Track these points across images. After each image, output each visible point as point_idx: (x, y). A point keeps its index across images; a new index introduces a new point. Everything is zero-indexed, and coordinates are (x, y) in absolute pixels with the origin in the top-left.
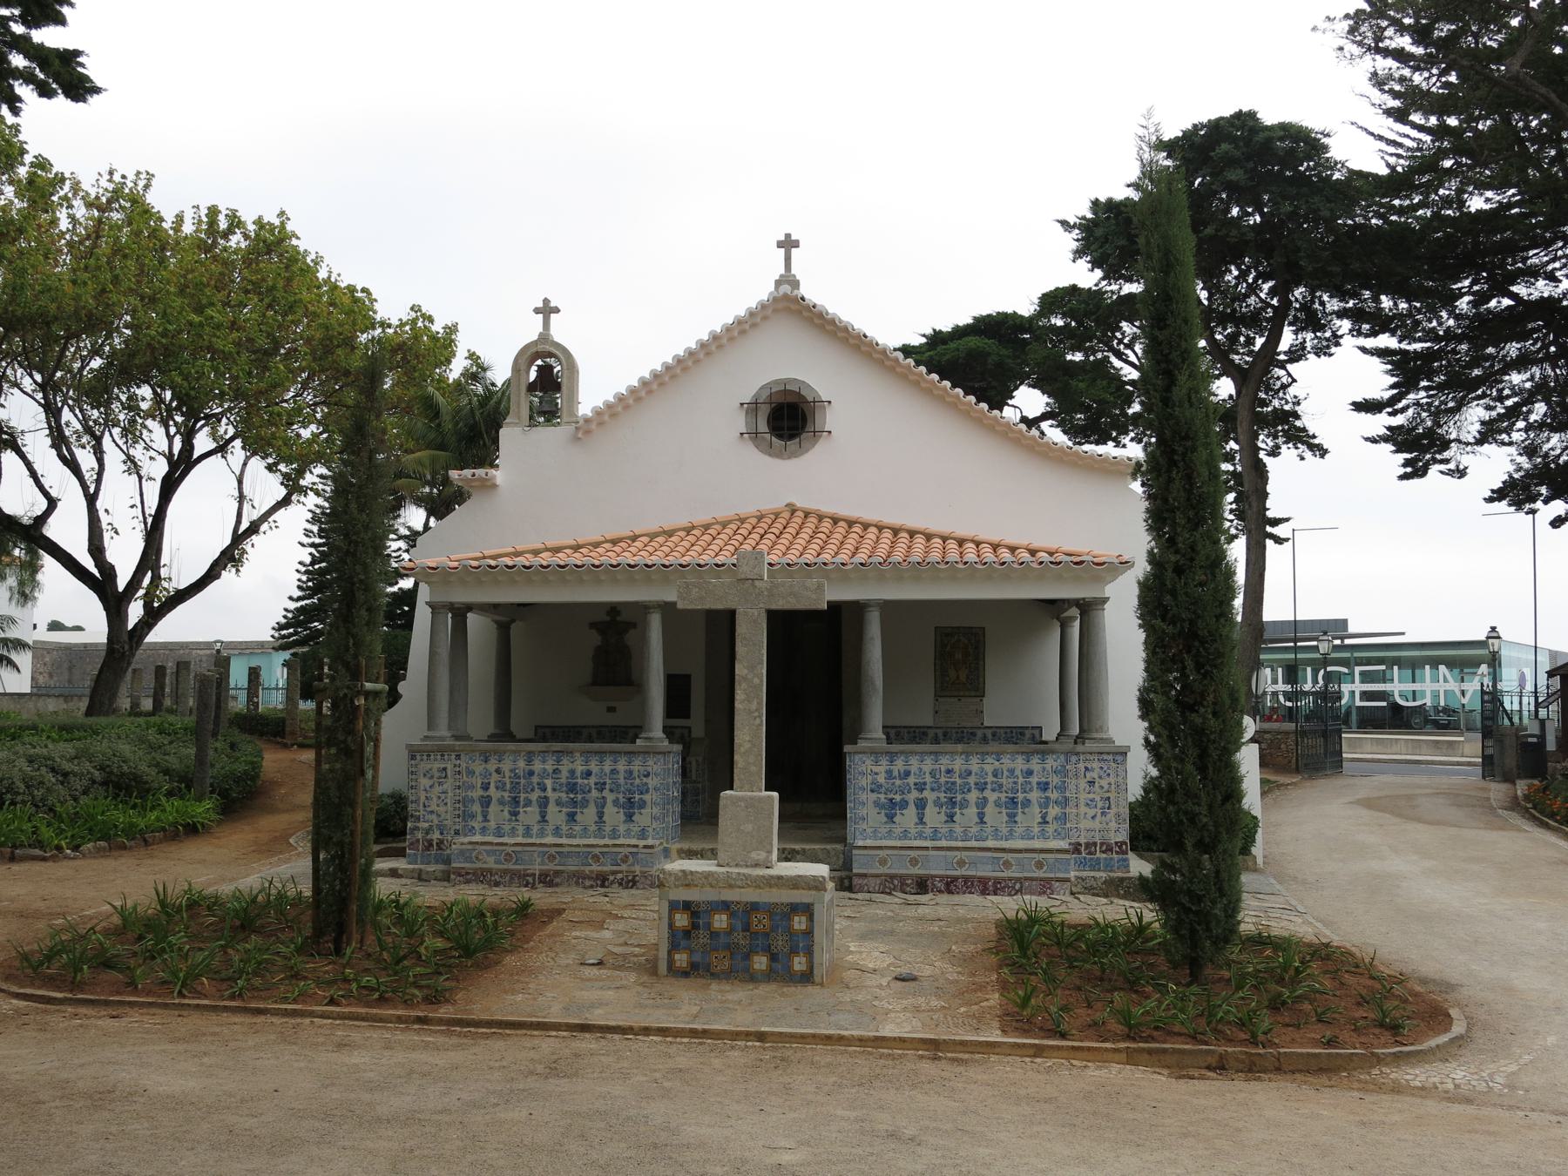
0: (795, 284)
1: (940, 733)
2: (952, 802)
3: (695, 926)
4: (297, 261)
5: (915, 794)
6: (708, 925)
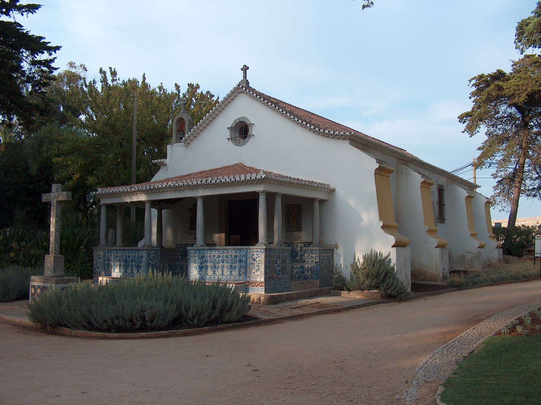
0: (248, 83)
2: (215, 267)
4: (78, 93)
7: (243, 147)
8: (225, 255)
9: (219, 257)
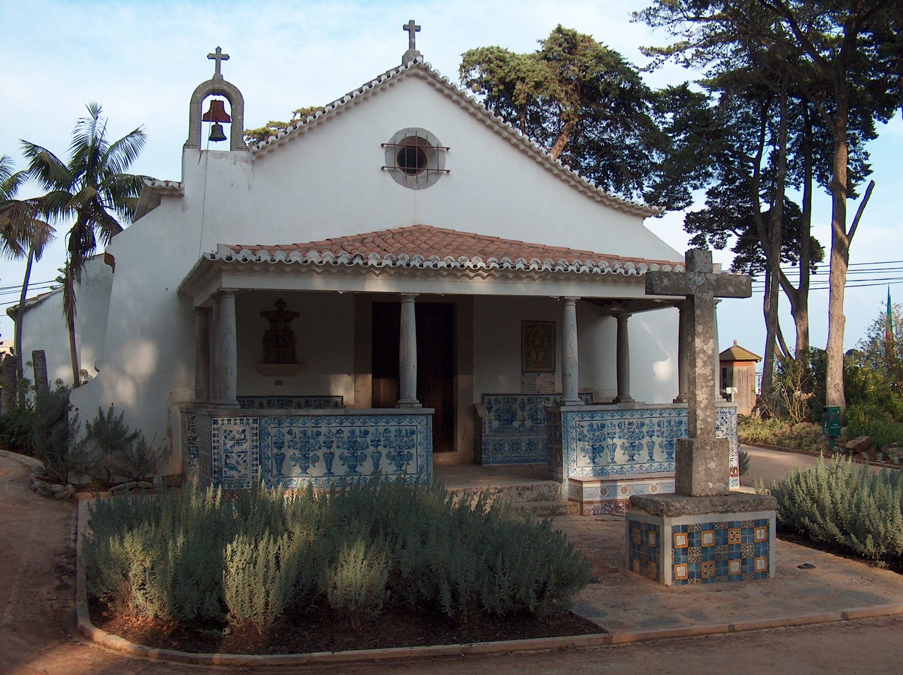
1: (302, 400)
3: (690, 544)
5: (647, 439)
6: (700, 542)
7: (422, 192)
8: (655, 421)
9: (643, 425)
